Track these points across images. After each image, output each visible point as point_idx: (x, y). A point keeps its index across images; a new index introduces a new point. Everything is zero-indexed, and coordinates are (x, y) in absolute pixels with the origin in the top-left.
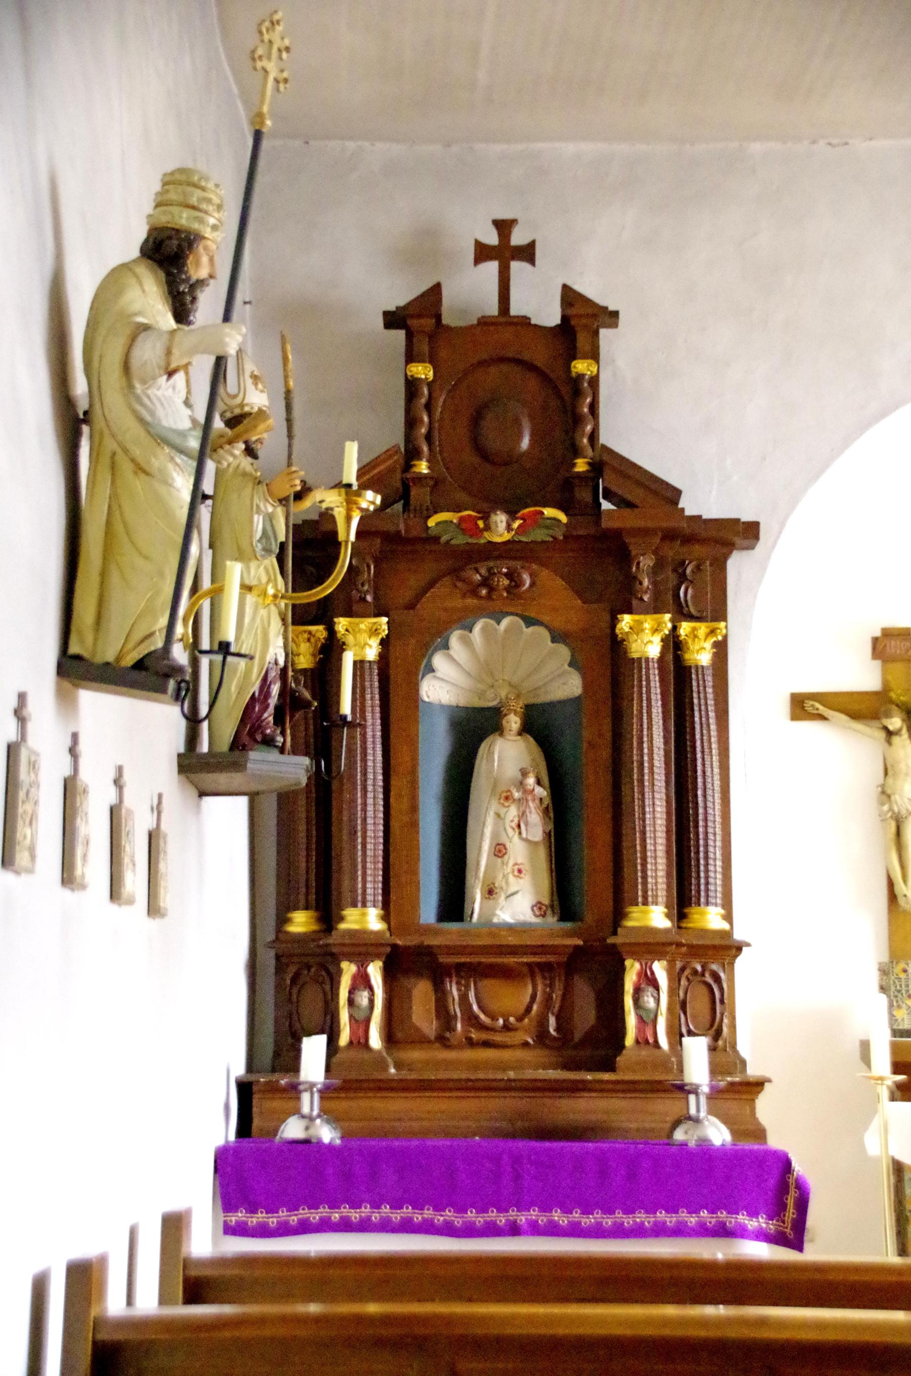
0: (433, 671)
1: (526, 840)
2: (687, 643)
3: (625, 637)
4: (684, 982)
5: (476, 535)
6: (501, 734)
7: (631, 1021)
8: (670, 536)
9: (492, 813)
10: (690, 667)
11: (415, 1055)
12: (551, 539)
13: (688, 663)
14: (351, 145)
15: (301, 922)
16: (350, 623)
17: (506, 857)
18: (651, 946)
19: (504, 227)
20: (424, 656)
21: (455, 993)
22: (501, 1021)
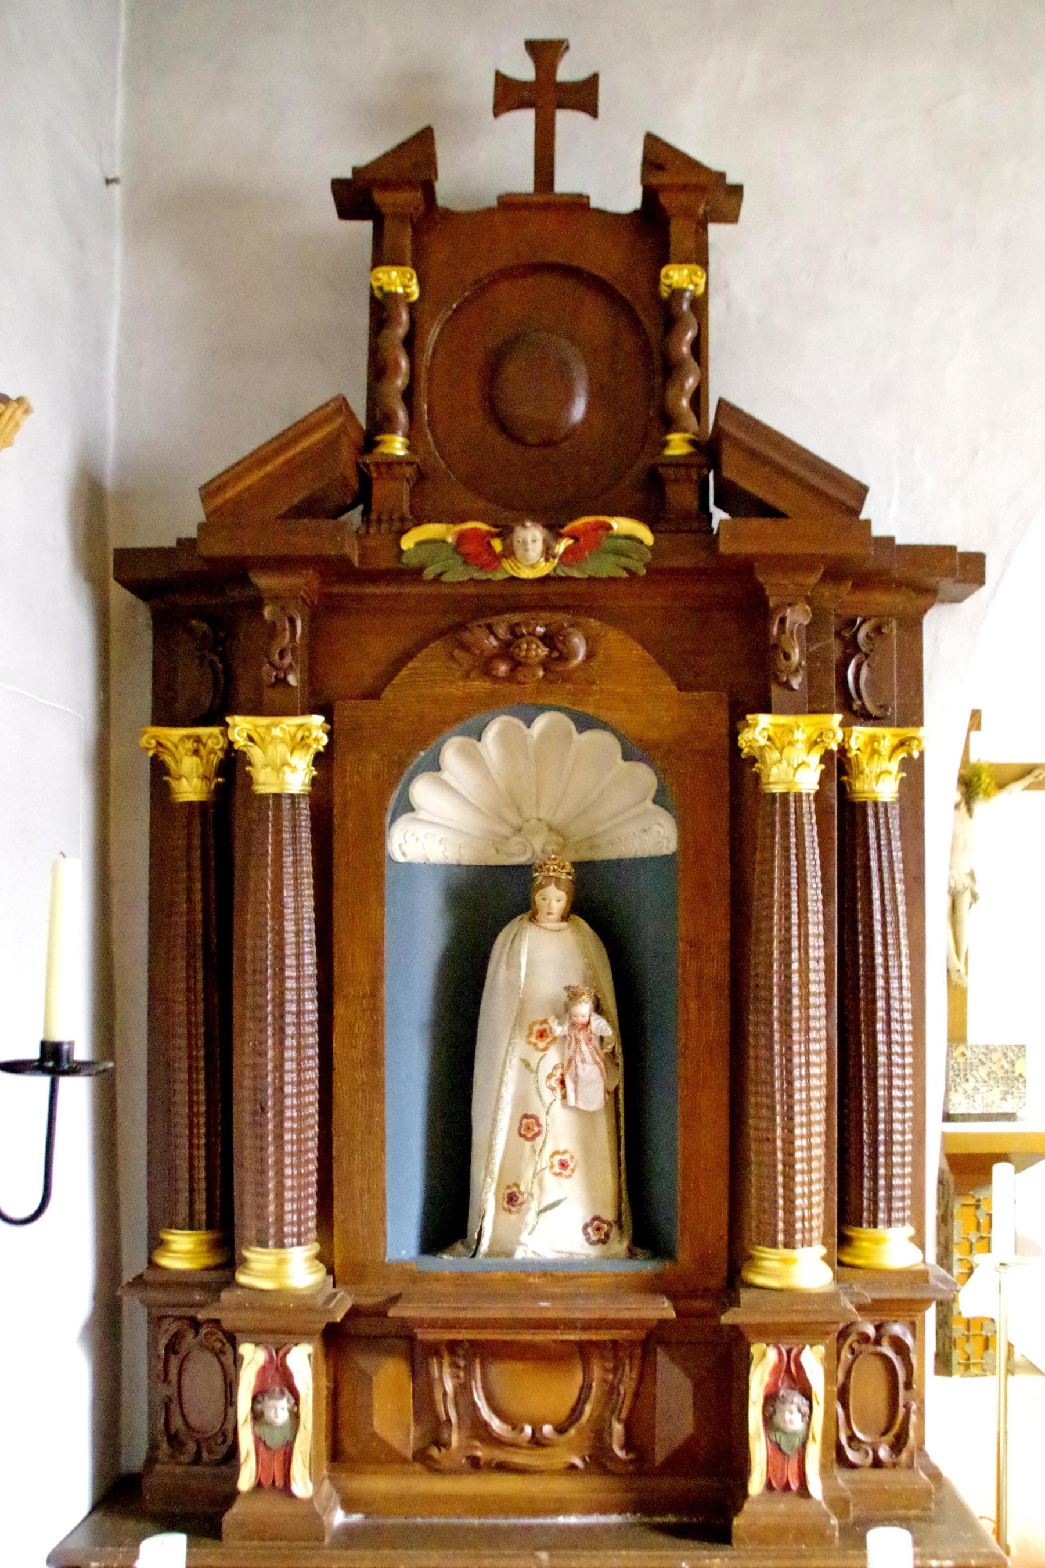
0: (412, 810)
1: (575, 1109)
2: (858, 765)
3: (757, 755)
4: (846, 1355)
5: (488, 565)
6: (533, 919)
8: (836, 572)
9: (515, 1062)
10: (864, 805)
11: (378, 1484)
12: (625, 575)
13: (859, 798)
15: (184, 1251)
16: (255, 727)
17: (540, 1140)
19: (544, 52)
20: (392, 785)
21: (449, 1386)
22: (528, 1430)
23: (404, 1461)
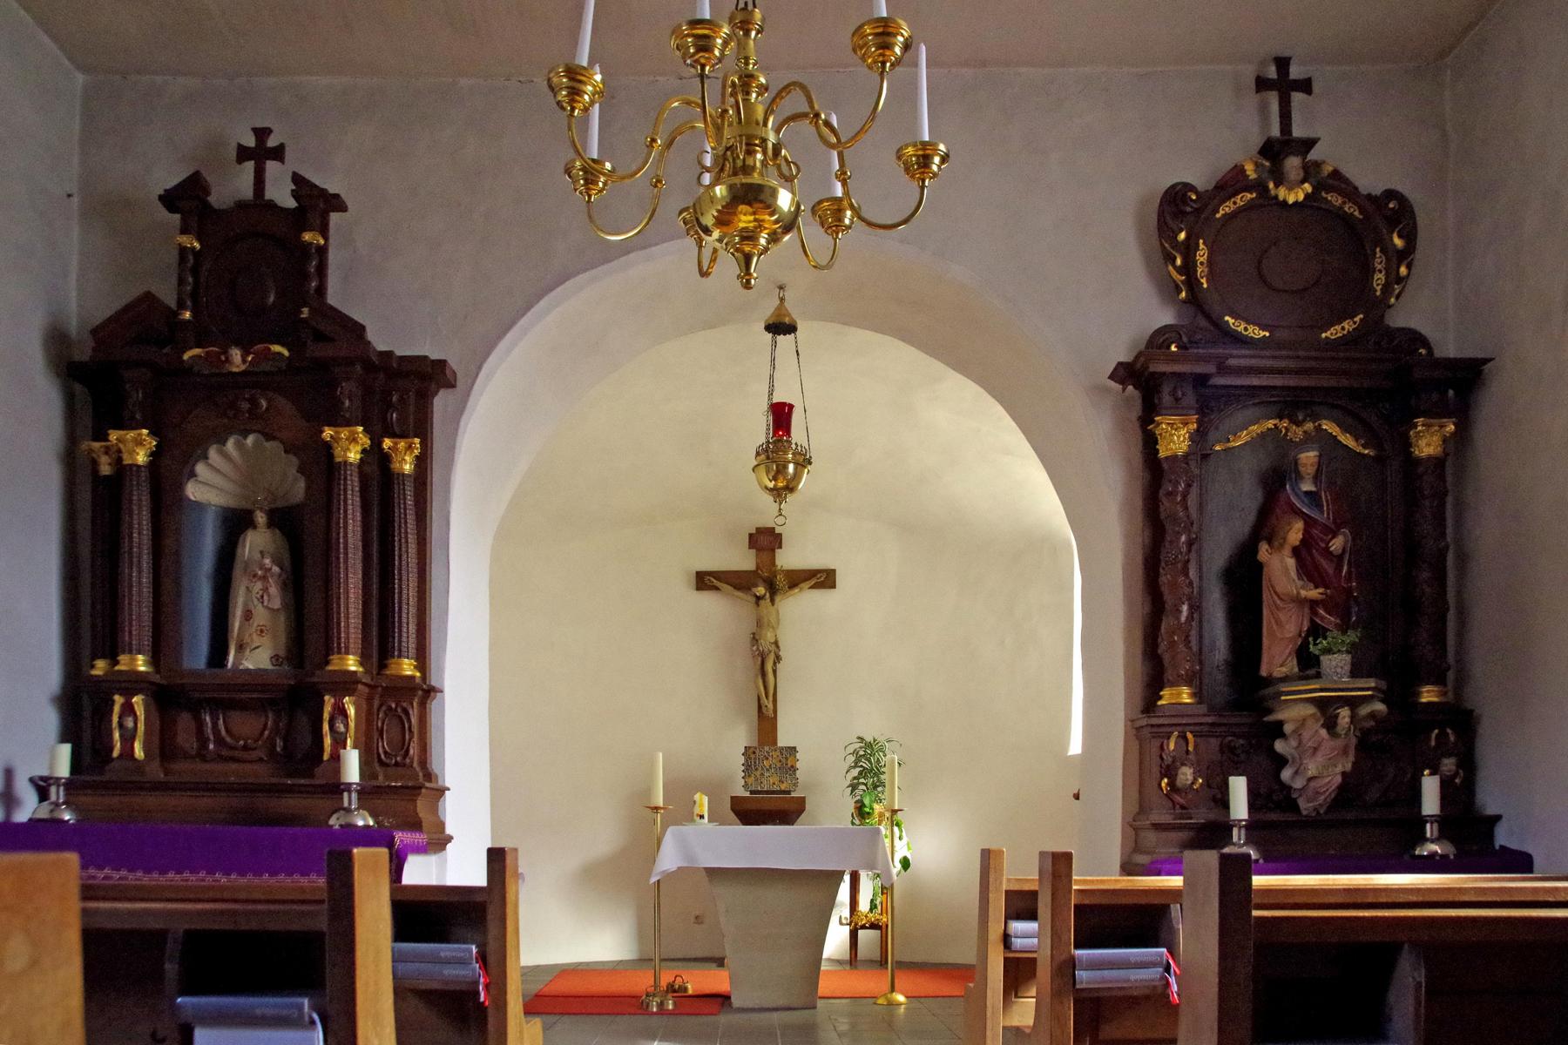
7: (328, 741)
14: (159, 79)
18: (346, 684)
19: (262, 133)
23: (192, 757)
